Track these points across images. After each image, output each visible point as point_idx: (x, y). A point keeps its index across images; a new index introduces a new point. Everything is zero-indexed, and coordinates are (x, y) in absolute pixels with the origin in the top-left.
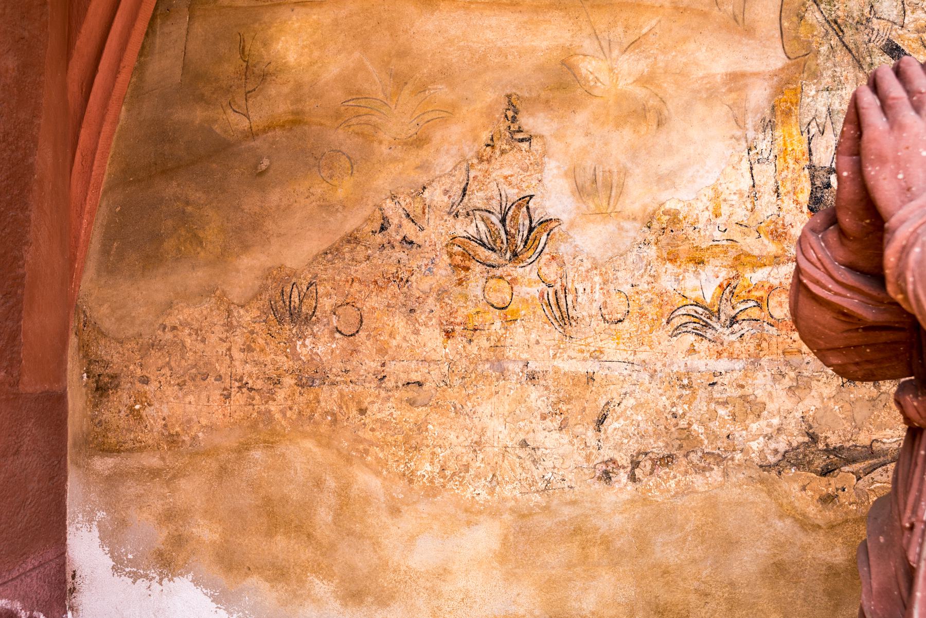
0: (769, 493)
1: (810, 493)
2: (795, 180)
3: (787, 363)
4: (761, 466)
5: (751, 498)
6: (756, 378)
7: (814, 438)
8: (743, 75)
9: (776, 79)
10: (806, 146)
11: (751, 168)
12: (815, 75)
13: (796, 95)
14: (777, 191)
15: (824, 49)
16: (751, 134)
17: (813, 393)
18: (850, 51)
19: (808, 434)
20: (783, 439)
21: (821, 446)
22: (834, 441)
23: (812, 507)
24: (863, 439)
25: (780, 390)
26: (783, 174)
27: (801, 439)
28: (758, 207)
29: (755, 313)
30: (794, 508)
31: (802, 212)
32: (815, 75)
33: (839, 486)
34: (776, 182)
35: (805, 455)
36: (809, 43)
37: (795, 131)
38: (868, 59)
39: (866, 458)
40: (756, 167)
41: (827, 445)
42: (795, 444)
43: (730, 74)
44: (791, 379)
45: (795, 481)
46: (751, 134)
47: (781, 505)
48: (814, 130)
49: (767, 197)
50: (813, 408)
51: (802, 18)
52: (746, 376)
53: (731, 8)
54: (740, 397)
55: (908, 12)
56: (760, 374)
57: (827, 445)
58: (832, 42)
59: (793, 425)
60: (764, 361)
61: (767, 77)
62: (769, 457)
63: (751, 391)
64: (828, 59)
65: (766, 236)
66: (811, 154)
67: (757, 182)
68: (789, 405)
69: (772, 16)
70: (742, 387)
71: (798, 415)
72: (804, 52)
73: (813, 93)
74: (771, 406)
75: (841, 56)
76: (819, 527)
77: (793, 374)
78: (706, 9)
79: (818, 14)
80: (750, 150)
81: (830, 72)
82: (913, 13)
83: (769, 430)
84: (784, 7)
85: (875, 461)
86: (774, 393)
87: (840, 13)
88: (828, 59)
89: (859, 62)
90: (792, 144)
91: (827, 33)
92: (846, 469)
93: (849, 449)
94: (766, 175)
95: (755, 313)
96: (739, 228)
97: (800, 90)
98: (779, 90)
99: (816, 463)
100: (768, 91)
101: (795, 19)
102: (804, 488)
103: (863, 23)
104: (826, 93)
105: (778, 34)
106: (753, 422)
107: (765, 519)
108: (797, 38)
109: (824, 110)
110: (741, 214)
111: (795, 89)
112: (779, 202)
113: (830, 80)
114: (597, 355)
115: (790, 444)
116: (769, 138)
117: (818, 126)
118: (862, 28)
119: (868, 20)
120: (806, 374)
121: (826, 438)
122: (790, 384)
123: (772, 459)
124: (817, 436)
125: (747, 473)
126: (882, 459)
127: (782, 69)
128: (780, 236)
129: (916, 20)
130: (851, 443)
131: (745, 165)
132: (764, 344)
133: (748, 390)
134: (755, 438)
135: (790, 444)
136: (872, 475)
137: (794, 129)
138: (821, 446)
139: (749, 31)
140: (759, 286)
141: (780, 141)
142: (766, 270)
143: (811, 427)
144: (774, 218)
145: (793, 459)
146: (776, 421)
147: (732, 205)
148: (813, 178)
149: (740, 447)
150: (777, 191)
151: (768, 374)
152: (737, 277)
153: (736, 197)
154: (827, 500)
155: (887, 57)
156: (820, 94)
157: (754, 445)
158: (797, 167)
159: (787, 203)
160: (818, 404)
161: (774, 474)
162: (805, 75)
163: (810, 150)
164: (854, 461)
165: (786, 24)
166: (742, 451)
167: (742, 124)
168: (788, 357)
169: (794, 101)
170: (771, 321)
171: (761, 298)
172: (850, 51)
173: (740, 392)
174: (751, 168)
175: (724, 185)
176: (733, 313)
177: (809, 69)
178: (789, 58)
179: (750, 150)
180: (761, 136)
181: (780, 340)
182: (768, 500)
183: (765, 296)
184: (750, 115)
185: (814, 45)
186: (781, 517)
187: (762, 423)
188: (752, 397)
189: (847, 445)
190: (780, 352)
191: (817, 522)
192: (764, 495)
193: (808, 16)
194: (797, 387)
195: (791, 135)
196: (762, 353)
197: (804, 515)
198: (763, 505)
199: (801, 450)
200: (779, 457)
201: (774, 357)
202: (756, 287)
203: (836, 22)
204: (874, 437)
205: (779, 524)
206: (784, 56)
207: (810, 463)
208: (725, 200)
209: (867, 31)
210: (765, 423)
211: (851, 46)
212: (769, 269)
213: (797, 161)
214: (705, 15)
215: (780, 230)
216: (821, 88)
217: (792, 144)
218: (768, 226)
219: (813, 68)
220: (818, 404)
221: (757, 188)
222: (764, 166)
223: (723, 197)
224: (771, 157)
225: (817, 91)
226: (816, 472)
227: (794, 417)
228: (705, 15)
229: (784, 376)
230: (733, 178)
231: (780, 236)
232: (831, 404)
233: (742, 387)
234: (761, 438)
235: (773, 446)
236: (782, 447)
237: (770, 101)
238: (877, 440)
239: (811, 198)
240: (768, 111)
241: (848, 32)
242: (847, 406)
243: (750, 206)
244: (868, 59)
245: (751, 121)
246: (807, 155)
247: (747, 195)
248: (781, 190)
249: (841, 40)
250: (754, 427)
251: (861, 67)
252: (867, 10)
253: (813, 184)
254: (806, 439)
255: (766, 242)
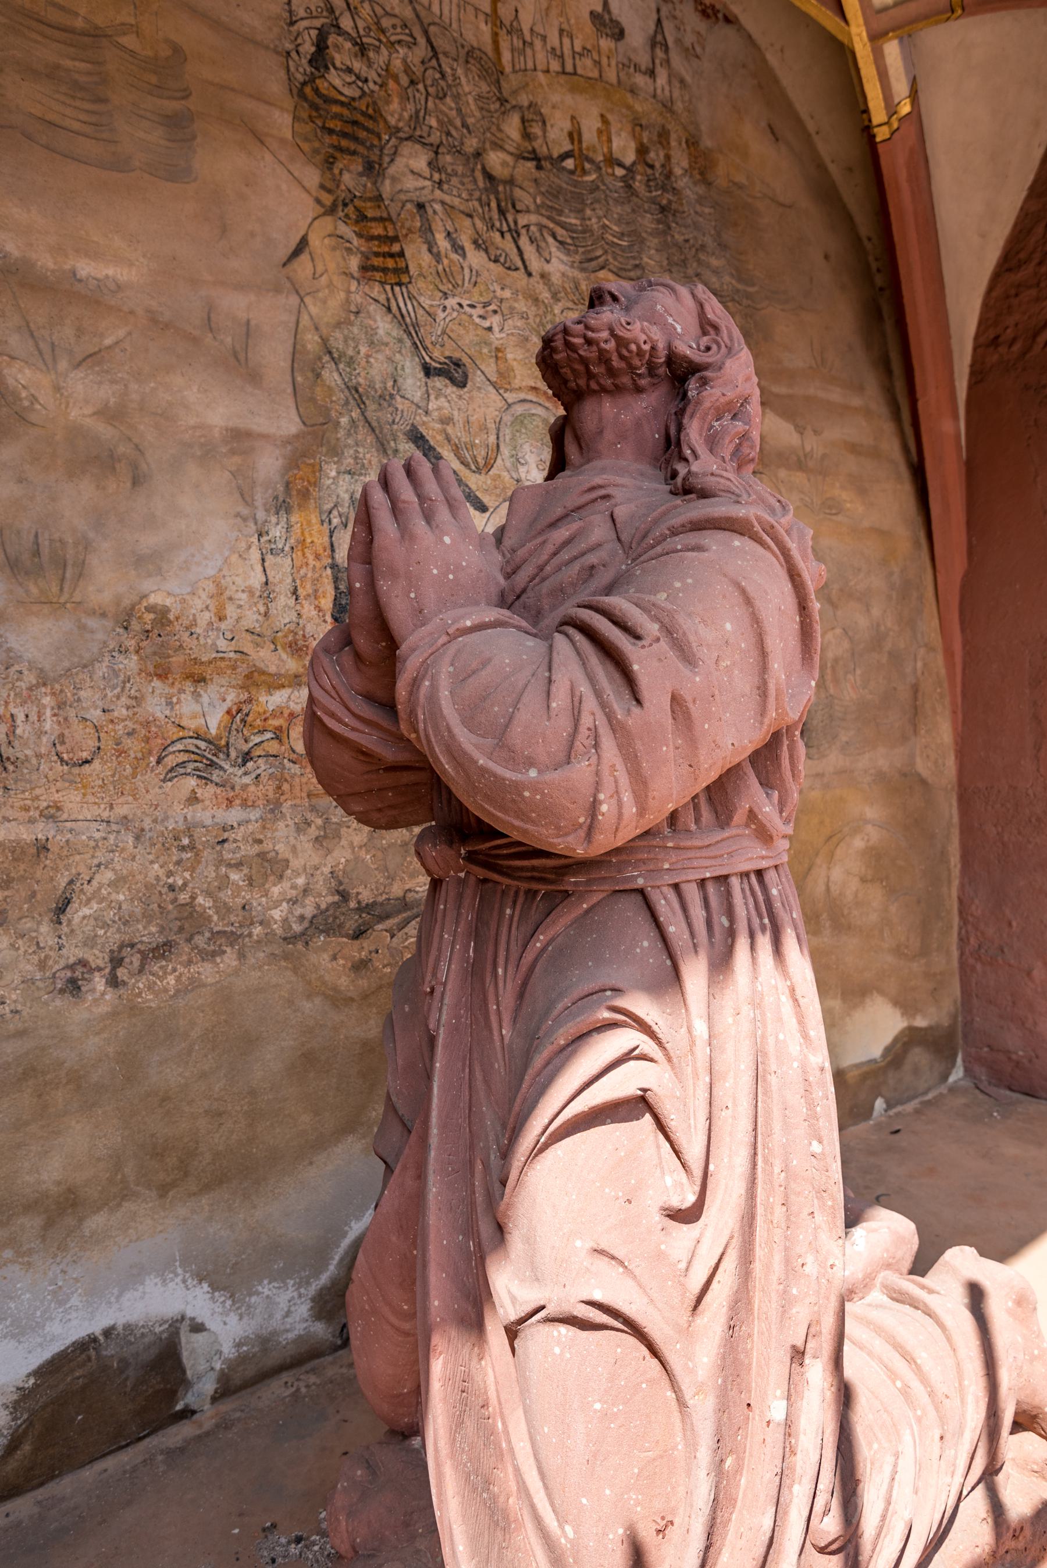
0: (295, 970)
1: (341, 962)
2: (316, 581)
3: (313, 809)
4: (285, 939)
5: (274, 981)
6: (277, 830)
7: (344, 896)
8: (248, 434)
9: (289, 448)
10: (326, 539)
11: (263, 560)
12: (335, 452)
13: (314, 472)
14: (295, 592)
15: (344, 420)
16: (261, 515)
17: (344, 842)
18: (373, 430)
19: (338, 892)
20: (310, 901)
21: (353, 904)
22: (366, 896)
23: (343, 978)
24: (397, 890)
25: (305, 843)
26: (302, 572)
27: (330, 899)
28: (273, 612)
29: (273, 747)
30: (324, 983)
31: (325, 621)
32: (335, 452)
33: (372, 948)
34: (294, 581)
35: (336, 918)
36: (328, 410)
37: (314, 519)
38: (392, 444)
39: (399, 912)
40: (269, 558)
41: (359, 902)
42: (323, 906)
43: (232, 430)
44: (318, 828)
45: (325, 950)
46: (261, 515)
47: (309, 983)
48: (336, 521)
49: (284, 600)
50: (343, 860)
51: (318, 376)
52: (264, 828)
53: (229, 340)
54: (258, 855)
55: (432, 397)
56: (281, 824)
57: (359, 902)
58: (353, 414)
59: (320, 884)
60: (286, 807)
61: (278, 443)
62: (294, 926)
63: (271, 846)
64: (349, 435)
65: (284, 649)
66: (333, 551)
67: (271, 579)
68: (316, 860)
69: (282, 364)
70: (260, 842)
71: (326, 870)
72: (321, 420)
73: (333, 474)
74: (296, 863)
75: (362, 430)
76: (352, 999)
77: (319, 822)
78: (197, 333)
79: (336, 375)
80: (260, 535)
81: (352, 452)
82: (436, 398)
83: (294, 892)
84: (297, 356)
85: (409, 913)
86: (299, 847)
87: (361, 380)
88: (349, 435)
89: (382, 445)
90: (311, 535)
91: (347, 403)
92: (380, 927)
93: (382, 904)
94: (281, 569)
95: (273, 747)
96: (249, 637)
97: (317, 467)
98: (293, 462)
99: (347, 925)
100: (280, 462)
101: (310, 375)
102: (334, 958)
103: (386, 398)
104: (347, 477)
105: (290, 390)
106: (275, 885)
107: (290, 1002)
108: (312, 400)
109: (347, 497)
110: (251, 618)
111: (313, 465)
112: (298, 607)
113: (352, 461)
114: (52, 814)
115: (318, 906)
116: (283, 523)
117: (340, 516)
118: (385, 404)
119: (391, 396)
120: (334, 820)
121: (358, 894)
122: (317, 833)
123: (297, 928)
124: (348, 894)
125: (268, 950)
126: (415, 911)
127: (297, 437)
128: (301, 649)
129: (439, 409)
130: (384, 896)
131: (255, 555)
132: (286, 787)
133: (267, 846)
134: (277, 904)
135: (318, 906)
136: (406, 930)
137: (313, 516)
138: (353, 904)
139: (254, 377)
140: (278, 712)
141: (297, 529)
142: (285, 693)
143: (341, 883)
144: (292, 626)
145: (323, 924)
146: (301, 881)
147: (240, 607)
148: (336, 580)
149: (260, 918)
150: (295, 592)
151: (290, 822)
152: (250, 701)
153: (244, 596)
154: (360, 966)
155: (412, 446)
156: (341, 477)
157: (277, 914)
158: (318, 565)
159: (308, 609)
160: (350, 856)
161: (300, 946)
162: (324, 449)
163: (332, 545)
164: (388, 917)
165: (299, 379)
166: (261, 923)
167: (248, 499)
168: (314, 801)
169: (313, 480)
170: (294, 756)
171: (279, 729)
172: (373, 430)
173: (256, 849)
174: (263, 560)
175: (228, 579)
176: (245, 748)
177: (329, 442)
178: (304, 423)
179: (260, 535)
180: (274, 519)
181: (304, 780)
182: (294, 979)
183: (285, 725)
184: (259, 489)
185: (333, 414)
186: (309, 997)
187: (286, 884)
188: (273, 854)
189: (380, 899)
190: (304, 795)
191: (349, 994)
192: (289, 973)
193: (326, 374)
194: (325, 837)
195: (309, 523)
196: (283, 798)
197: (335, 989)
198: (289, 986)
199: (331, 912)
200: (306, 924)
201: (298, 801)
202: (274, 715)
203: (357, 391)
204: (407, 887)
205: (307, 1006)
206: (298, 420)
207: (340, 926)
208: (230, 599)
209: (390, 409)
210: (289, 885)
211: (374, 424)
212: (288, 691)
213: (317, 557)
214: (195, 341)
215: (301, 643)
216: (343, 469)
217: (311, 535)
218: (286, 636)
219: (333, 442)
220: (350, 856)
221: (271, 587)
222: (279, 559)
223: (228, 593)
224: (287, 549)
225: (338, 473)
226: (347, 936)
227: (322, 874)
228: (195, 341)
229: (309, 825)
230: (241, 571)
231: (301, 649)
232: (363, 853)
233: (260, 842)
234: (284, 904)
235: (298, 911)
236: (309, 911)
237: (283, 476)
238: (410, 890)
239: (335, 605)
240: (281, 488)
241: (371, 406)
242: (379, 854)
243: (262, 609)
244: (392, 444)
245: (260, 498)
246: (329, 551)
247: (258, 594)
248: (300, 591)
249: (363, 413)
250: (276, 890)
251: (385, 451)
252: (390, 384)
253: (336, 588)
254: (337, 898)
255: (284, 656)
